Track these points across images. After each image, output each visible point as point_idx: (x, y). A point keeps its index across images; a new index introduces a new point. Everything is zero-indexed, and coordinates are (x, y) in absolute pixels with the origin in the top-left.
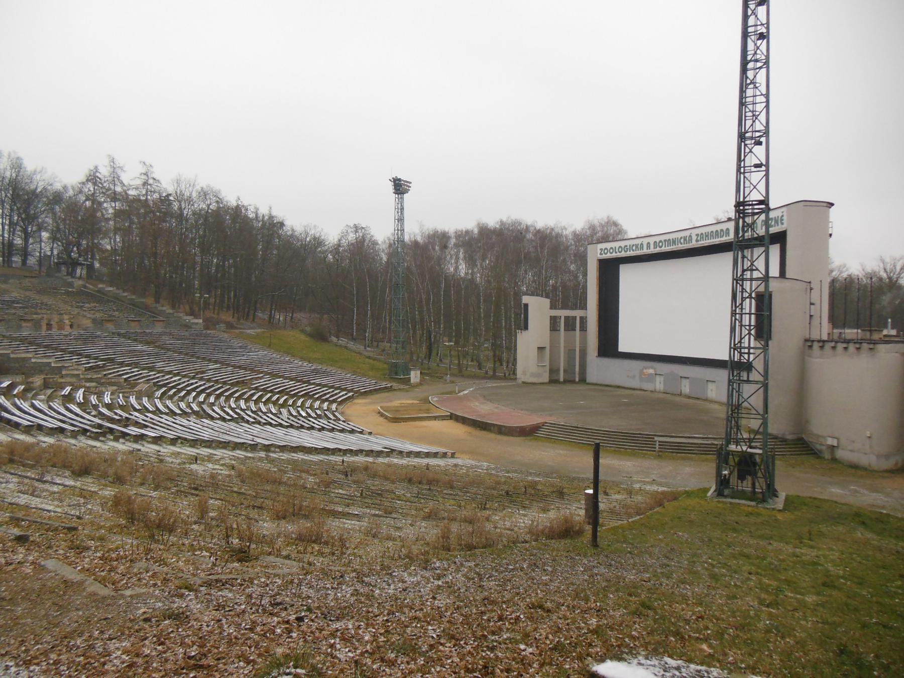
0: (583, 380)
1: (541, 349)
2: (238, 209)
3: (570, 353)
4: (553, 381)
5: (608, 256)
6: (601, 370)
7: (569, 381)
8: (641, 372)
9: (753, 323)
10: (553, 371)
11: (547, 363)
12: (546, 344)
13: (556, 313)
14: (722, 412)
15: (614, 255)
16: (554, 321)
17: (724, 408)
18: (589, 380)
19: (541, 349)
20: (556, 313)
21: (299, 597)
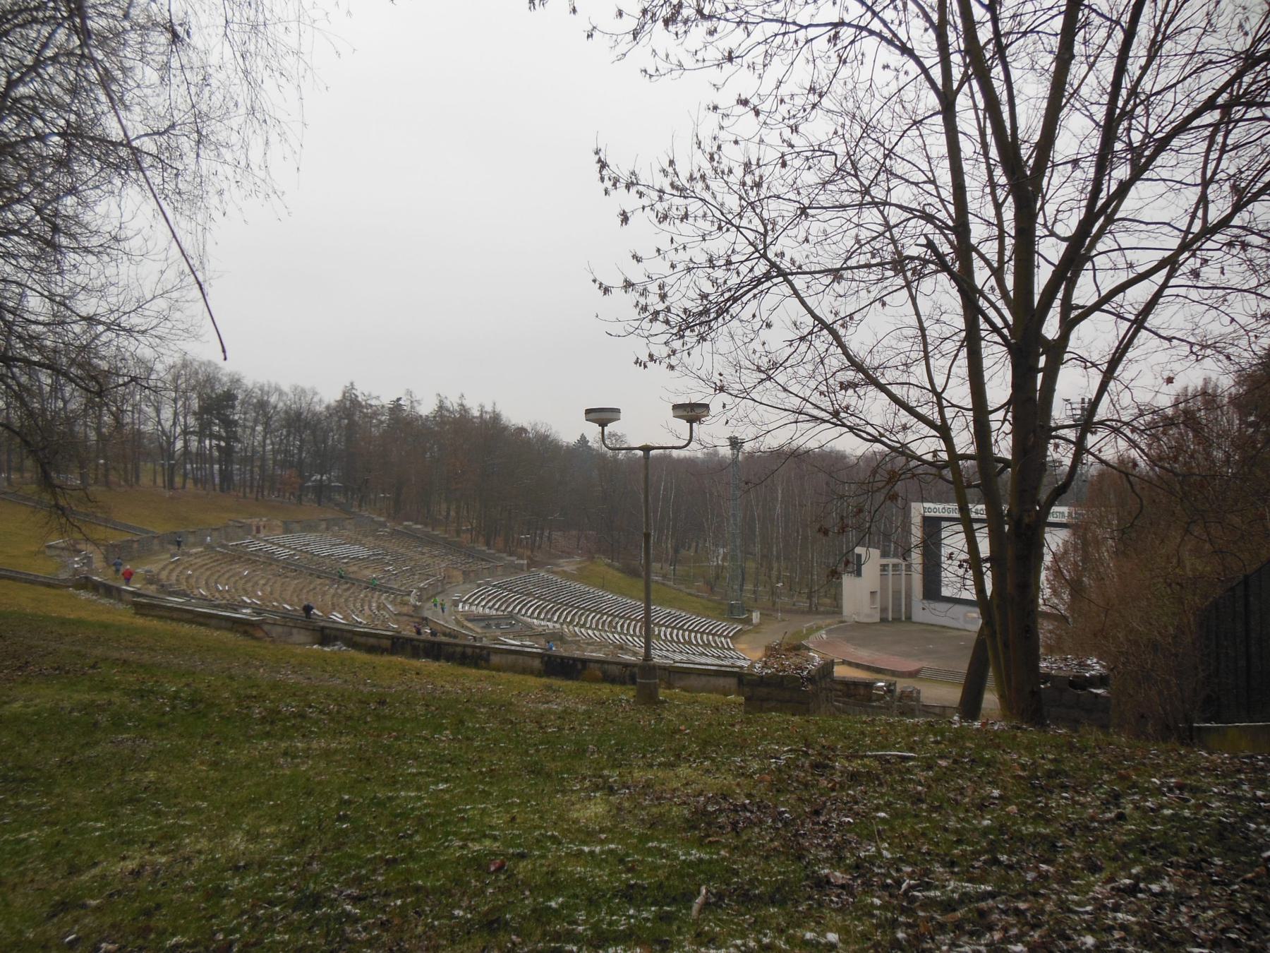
0: (909, 618)
1: (873, 593)
2: (396, 407)
3: (897, 594)
4: (883, 620)
5: (932, 514)
6: (924, 612)
7: (897, 620)
8: (965, 615)
9: (984, 548)
10: (884, 610)
11: (878, 605)
12: (877, 588)
13: (885, 561)
14: (643, 461)
15: (937, 514)
16: (884, 568)
17: (975, 613)
18: (915, 618)
19: (873, 593)
20: (885, 561)
21: (388, 862)
